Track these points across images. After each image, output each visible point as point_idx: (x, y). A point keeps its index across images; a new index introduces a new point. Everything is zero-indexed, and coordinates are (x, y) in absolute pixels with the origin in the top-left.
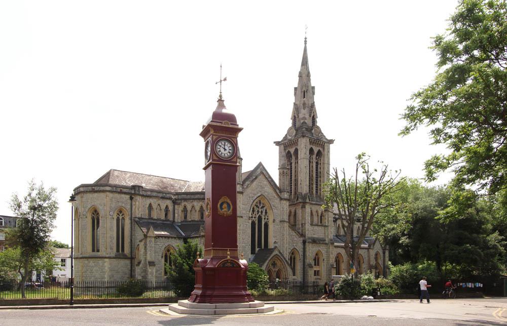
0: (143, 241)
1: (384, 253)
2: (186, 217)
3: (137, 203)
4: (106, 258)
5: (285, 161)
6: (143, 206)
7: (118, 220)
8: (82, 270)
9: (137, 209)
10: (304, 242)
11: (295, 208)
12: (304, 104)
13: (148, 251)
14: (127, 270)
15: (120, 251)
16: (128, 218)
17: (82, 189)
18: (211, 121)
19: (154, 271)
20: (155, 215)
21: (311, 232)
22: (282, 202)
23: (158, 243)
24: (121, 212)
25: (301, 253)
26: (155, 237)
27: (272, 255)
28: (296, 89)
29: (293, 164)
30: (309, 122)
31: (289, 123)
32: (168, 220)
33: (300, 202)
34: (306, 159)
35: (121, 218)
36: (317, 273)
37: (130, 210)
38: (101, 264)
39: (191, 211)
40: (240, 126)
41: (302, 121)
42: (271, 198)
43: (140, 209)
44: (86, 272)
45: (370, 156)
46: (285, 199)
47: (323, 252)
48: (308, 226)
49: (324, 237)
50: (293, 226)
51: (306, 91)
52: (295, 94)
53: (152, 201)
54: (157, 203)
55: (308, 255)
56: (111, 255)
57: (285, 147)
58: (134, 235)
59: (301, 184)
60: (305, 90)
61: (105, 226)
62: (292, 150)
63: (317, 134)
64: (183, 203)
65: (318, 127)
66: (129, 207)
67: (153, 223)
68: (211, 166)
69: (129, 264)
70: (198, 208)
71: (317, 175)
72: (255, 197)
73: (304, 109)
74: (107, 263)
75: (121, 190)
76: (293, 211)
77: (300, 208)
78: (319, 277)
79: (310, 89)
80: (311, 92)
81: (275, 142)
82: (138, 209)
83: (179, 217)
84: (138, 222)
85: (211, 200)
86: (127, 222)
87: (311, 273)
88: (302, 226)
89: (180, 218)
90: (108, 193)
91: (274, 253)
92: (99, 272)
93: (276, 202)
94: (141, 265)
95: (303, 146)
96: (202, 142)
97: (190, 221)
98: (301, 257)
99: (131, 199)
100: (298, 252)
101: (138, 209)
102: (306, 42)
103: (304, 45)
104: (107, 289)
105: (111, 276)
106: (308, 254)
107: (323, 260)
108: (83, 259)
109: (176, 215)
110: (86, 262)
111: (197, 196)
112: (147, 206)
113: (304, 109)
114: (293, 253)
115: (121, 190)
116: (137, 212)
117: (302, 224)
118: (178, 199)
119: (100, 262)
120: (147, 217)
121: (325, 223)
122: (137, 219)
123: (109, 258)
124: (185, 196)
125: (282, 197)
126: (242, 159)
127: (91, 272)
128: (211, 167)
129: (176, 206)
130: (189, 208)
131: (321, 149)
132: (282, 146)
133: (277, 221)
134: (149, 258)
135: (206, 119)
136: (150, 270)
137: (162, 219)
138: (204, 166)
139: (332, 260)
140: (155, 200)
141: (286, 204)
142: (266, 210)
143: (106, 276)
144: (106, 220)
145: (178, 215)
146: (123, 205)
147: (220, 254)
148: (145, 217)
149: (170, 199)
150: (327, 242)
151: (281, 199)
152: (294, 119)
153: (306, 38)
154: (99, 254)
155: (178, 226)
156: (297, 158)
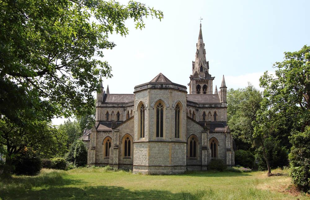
24: (160, 104)
35: (160, 109)
41: (206, 70)
57: (196, 82)
60: (201, 52)
102: (201, 26)
103: (200, 28)
108: (171, 143)
110: (174, 145)
111: (192, 104)
119: (182, 146)
126: (227, 88)
130: (207, 113)
131: (206, 85)
153: (201, 24)
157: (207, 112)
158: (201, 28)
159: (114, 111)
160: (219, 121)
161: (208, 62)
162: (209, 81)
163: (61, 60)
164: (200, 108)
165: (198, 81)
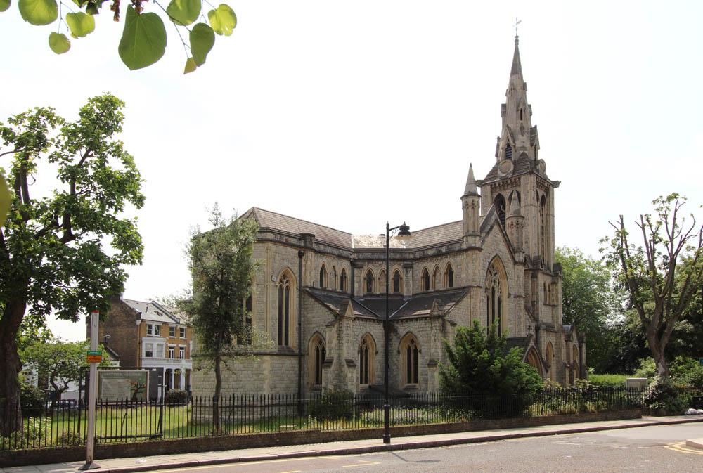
1: (581, 347)
2: (427, 287)
3: (309, 263)
4: (266, 354)
12: (522, 128)
16: (295, 287)
22: (517, 267)
24: (284, 276)
26: (355, 319)
37: (297, 274)
39: (435, 275)
41: (521, 152)
43: (312, 274)
45: (685, 199)
46: (521, 263)
52: (504, 114)
59: (526, 242)
62: (506, 194)
64: (367, 267)
66: (296, 269)
69: (297, 366)
70: (443, 269)
72: (491, 258)
74: (267, 364)
75: (287, 240)
77: (530, 278)
82: (310, 273)
83: (360, 290)
84: (307, 293)
86: (294, 294)
88: (533, 305)
89: (362, 289)
90: (271, 245)
92: (252, 379)
93: (510, 266)
94: (333, 366)
97: (378, 295)
99: (301, 255)
101: (310, 273)
102: (517, 42)
103: (514, 46)
104: (266, 409)
105: (273, 386)
109: (356, 285)
113: (522, 134)
116: (308, 277)
117: (533, 302)
118: (359, 260)
121: (553, 301)
123: (271, 354)
124: (369, 255)
129: (356, 270)
132: (488, 188)
134: (345, 355)
136: (349, 375)
143: (265, 386)
145: (360, 286)
146: (289, 265)
149: (347, 258)
150: (556, 329)
153: (517, 37)
157: (377, 271)
158: (519, 46)
159: (440, 266)
160: (458, 286)
161: (536, 126)
162: (523, 178)
163: (122, 200)
164: (416, 260)
165: (495, 185)
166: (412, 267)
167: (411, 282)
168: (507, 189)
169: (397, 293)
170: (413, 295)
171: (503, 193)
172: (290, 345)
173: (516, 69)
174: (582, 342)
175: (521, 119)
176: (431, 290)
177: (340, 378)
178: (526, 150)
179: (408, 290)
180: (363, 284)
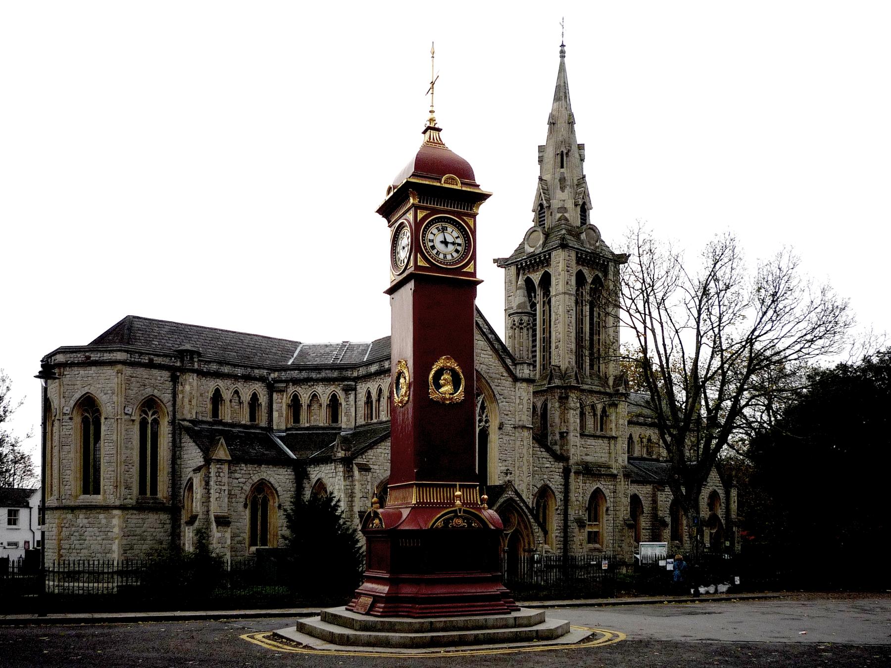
0: (203, 471)
2: (297, 419)
3: (187, 388)
5: (520, 298)
6: (201, 395)
7: (143, 424)
8: (60, 534)
9: (186, 400)
10: (566, 473)
11: (543, 398)
12: (562, 180)
13: (212, 491)
14: (162, 534)
15: (148, 495)
17: (60, 358)
18: (413, 175)
19: (228, 535)
20: (226, 415)
21: (580, 450)
22: (518, 384)
23: (237, 475)
25: (560, 496)
27: (501, 500)
28: (541, 149)
29: (538, 306)
30: (574, 216)
31: (528, 220)
32: (256, 427)
33: (557, 387)
34: (570, 294)
36: (593, 537)
38: (104, 521)
39: (309, 406)
40: (484, 188)
41: (559, 215)
42: (494, 376)
43: (194, 402)
44: (68, 538)
47: (607, 492)
48: (574, 439)
49: (607, 459)
50: (541, 437)
51: (567, 154)
52: (541, 160)
53: (221, 384)
54: (233, 387)
55: (574, 499)
56: (128, 501)
57: (518, 270)
58: (180, 458)
59: (557, 347)
61: (114, 438)
63: (592, 242)
64: (291, 389)
65: (593, 229)
66: (167, 397)
67: (221, 433)
68: (412, 282)
70: (325, 400)
71: (591, 329)
73: (562, 189)
74: (116, 520)
76: (539, 405)
78: (597, 546)
79: (574, 148)
80: (577, 156)
81: (495, 261)
85: (411, 363)
86: (165, 430)
87: (579, 537)
91: (505, 497)
92: (99, 538)
94: (197, 523)
95: (561, 266)
96: (383, 229)
98: (559, 503)
99: (174, 380)
100: (554, 493)
102: (563, 54)
105: (127, 549)
106: (573, 496)
107: (607, 510)
109: (275, 414)
110: (70, 516)
112: (211, 395)
113: (562, 189)
114: (544, 493)
115: (151, 360)
116: (187, 407)
117: (561, 434)
119: (101, 516)
120: (209, 419)
122: (186, 423)
123: (122, 508)
124: (295, 374)
125: (519, 375)
127: (82, 538)
128: (411, 285)
129: (275, 395)
130: (305, 399)
132: (513, 269)
133: (508, 428)
135: (398, 167)
137: (243, 422)
138: (388, 286)
139: (624, 512)
140: (228, 382)
141: (524, 392)
142: (483, 403)
144: (115, 426)
145: (280, 416)
147: (434, 497)
148: (204, 419)
151: (516, 379)
152: (541, 210)
154: (98, 499)
155: (280, 438)
156: (547, 293)
162: (554, 254)
166: (355, 389)
167: (353, 410)
168: (537, 270)
169: (334, 425)
170: (356, 427)
171: (531, 276)
172: (160, 495)
173: (562, 93)
174: (732, 486)
175: (562, 167)
176: (304, 423)
177: (202, 536)
178: (566, 212)
179: (348, 420)
180: (284, 413)
